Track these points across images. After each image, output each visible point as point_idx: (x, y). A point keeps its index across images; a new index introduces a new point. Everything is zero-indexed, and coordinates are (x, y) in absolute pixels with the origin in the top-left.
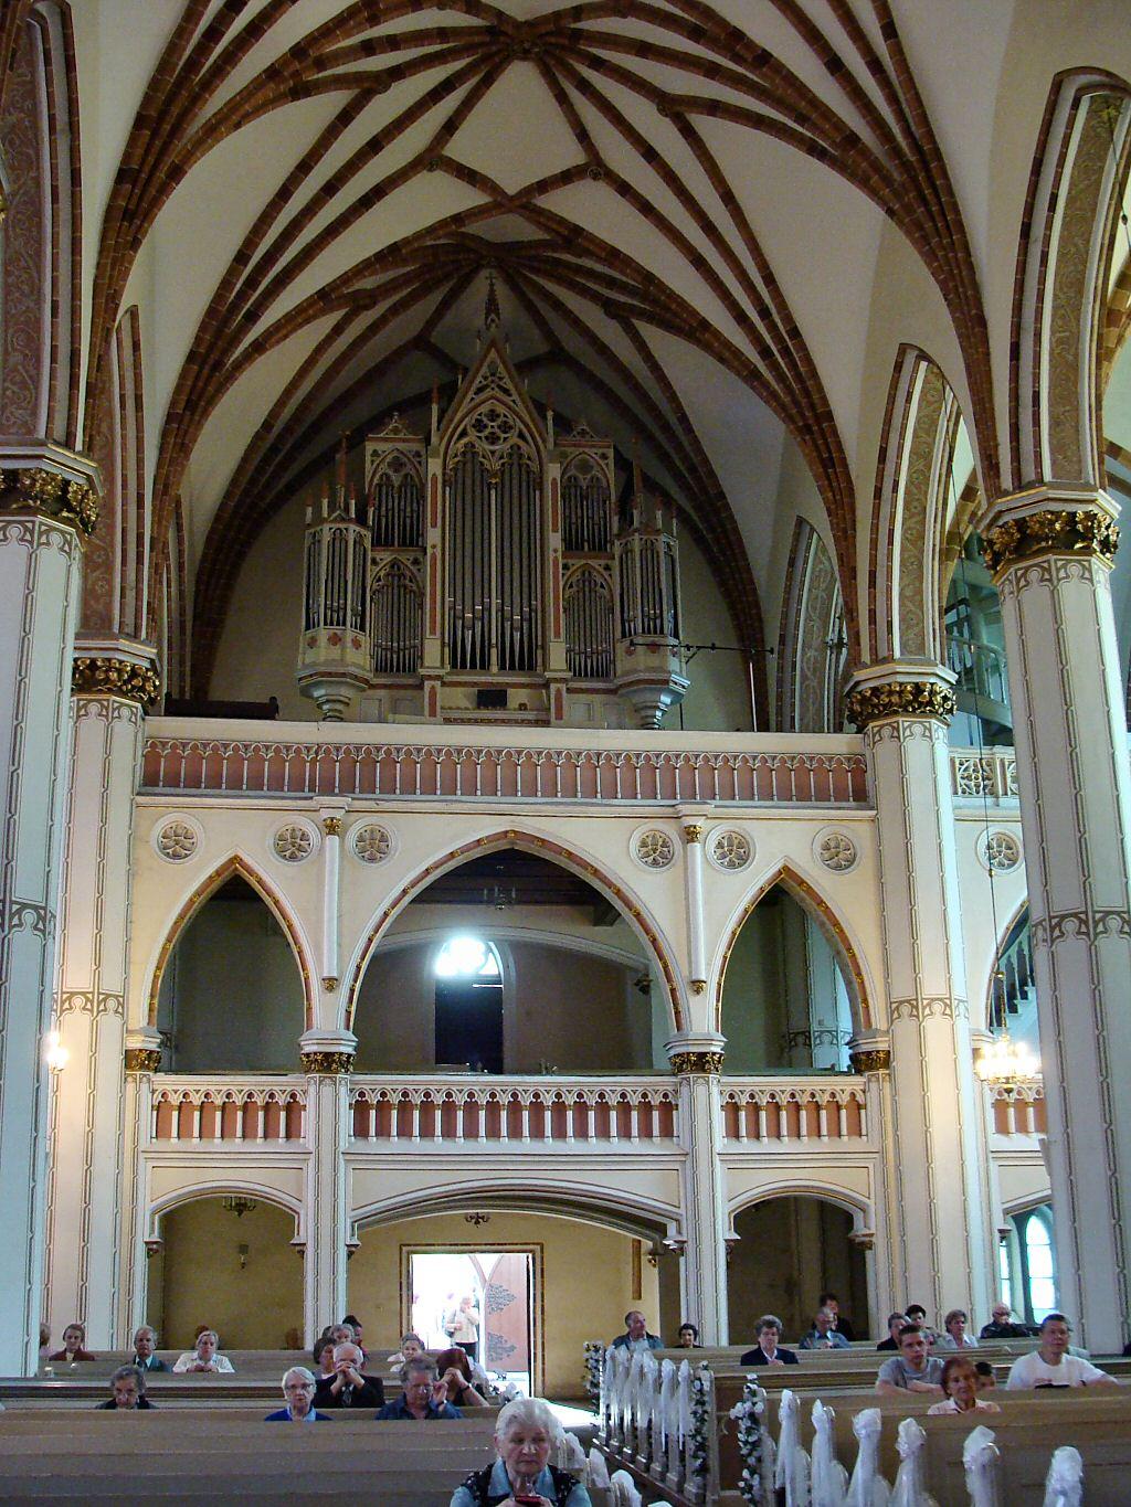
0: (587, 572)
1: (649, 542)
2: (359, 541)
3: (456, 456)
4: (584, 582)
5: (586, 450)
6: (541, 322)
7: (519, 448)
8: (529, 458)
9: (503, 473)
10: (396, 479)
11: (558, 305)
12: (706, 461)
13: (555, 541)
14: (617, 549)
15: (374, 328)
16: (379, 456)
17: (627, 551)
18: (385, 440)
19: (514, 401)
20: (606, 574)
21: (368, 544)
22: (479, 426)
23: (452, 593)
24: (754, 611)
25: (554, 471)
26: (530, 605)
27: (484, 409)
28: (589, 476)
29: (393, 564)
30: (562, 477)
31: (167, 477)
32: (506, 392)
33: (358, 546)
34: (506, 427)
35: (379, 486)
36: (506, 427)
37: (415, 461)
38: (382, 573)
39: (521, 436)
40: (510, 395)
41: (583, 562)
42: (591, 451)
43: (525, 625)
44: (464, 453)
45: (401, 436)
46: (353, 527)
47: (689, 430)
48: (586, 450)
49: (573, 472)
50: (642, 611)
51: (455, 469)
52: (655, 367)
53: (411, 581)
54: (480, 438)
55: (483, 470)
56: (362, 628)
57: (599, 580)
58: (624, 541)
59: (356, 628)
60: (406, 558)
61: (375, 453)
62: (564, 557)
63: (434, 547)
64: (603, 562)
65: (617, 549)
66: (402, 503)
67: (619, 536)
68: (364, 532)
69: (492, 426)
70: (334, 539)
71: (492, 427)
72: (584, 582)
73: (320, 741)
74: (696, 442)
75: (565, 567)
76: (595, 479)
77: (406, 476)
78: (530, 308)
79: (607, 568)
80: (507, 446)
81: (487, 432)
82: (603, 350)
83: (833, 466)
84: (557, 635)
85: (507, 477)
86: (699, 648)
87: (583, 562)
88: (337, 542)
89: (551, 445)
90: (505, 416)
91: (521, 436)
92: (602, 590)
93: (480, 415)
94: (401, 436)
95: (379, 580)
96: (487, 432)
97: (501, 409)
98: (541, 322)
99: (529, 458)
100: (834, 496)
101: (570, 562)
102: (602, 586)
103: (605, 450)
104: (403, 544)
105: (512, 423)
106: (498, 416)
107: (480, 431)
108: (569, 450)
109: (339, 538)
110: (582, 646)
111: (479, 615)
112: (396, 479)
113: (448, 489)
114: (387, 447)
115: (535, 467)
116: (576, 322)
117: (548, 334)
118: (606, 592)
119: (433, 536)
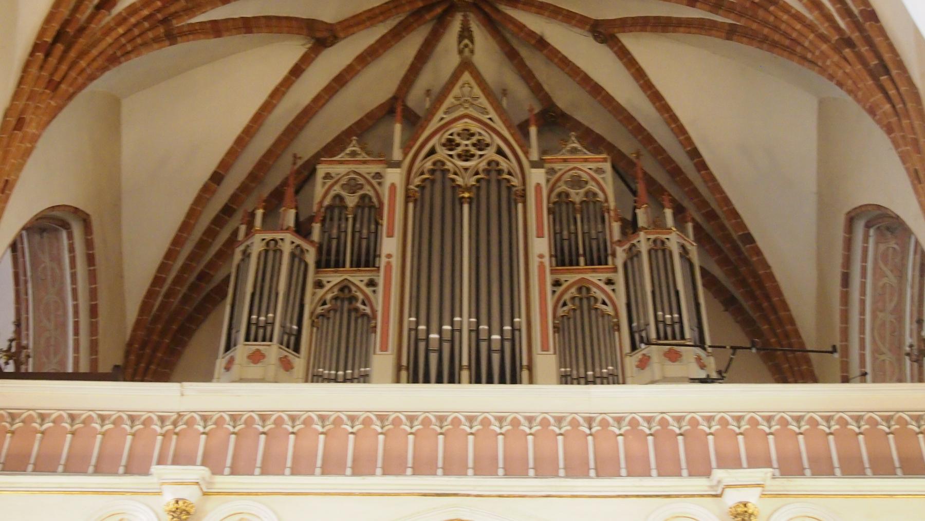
0: (583, 288)
1: (659, 243)
2: (297, 255)
3: (422, 173)
4: (581, 299)
5: (578, 165)
6: (527, 76)
7: (498, 164)
8: (510, 173)
9: (478, 188)
10: (351, 201)
11: (541, 44)
12: (726, 201)
13: (541, 247)
14: (621, 255)
15: (340, 81)
16: (332, 177)
17: (633, 255)
18: (341, 162)
19: (490, 119)
20: (608, 288)
21: (311, 257)
22: (450, 144)
23: (413, 312)
24: (804, 367)
25: (537, 176)
26: (512, 324)
27: (458, 127)
28: (582, 191)
29: (344, 287)
30: (551, 191)
31: (23, 111)
32: (484, 111)
33: (297, 260)
34: (481, 145)
35: (330, 208)
36: (481, 145)
37: (374, 182)
38: (329, 296)
39: (500, 152)
40: (487, 113)
41: (578, 277)
42: (585, 166)
43: (507, 345)
44: (432, 172)
45: (359, 158)
46: (289, 237)
47: (701, 166)
48: (578, 165)
49: (563, 187)
50: (656, 316)
51: (422, 187)
52: (656, 97)
53: (364, 303)
54: (451, 156)
55: (456, 188)
56: (297, 349)
57: (600, 296)
58: (627, 246)
59: (288, 347)
60: (359, 279)
61: (328, 176)
62: (553, 272)
63: (389, 256)
64: (604, 276)
65: (621, 255)
66: (358, 225)
67: (620, 243)
68: (305, 245)
69: (465, 144)
70: (266, 251)
71: (467, 145)
72: (581, 299)
73: (182, 408)
74: (715, 187)
75: (557, 283)
76: (591, 194)
77: (363, 197)
78: (512, 55)
79: (609, 282)
80: (483, 165)
81: (459, 150)
82: (596, 90)
83: (887, 71)
84: (545, 348)
85: (483, 193)
86: (734, 348)
87: (578, 277)
88: (271, 254)
89: (535, 156)
90: (480, 134)
91: (500, 152)
92: (604, 307)
93: (451, 135)
94: (359, 158)
95: (324, 303)
96: (459, 150)
97: (475, 127)
98: (527, 76)
99: (510, 173)
100: (894, 107)
101: (562, 277)
102: (604, 303)
103: (600, 165)
104: (357, 264)
105: (488, 140)
106: (473, 135)
107: (451, 150)
108: (557, 166)
109: (272, 250)
110: (582, 370)
111: (447, 336)
112: (351, 201)
113: (411, 205)
114: (342, 169)
115: (515, 181)
116: (565, 64)
117: (537, 89)
118: (609, 310)
119: (390, 246)
